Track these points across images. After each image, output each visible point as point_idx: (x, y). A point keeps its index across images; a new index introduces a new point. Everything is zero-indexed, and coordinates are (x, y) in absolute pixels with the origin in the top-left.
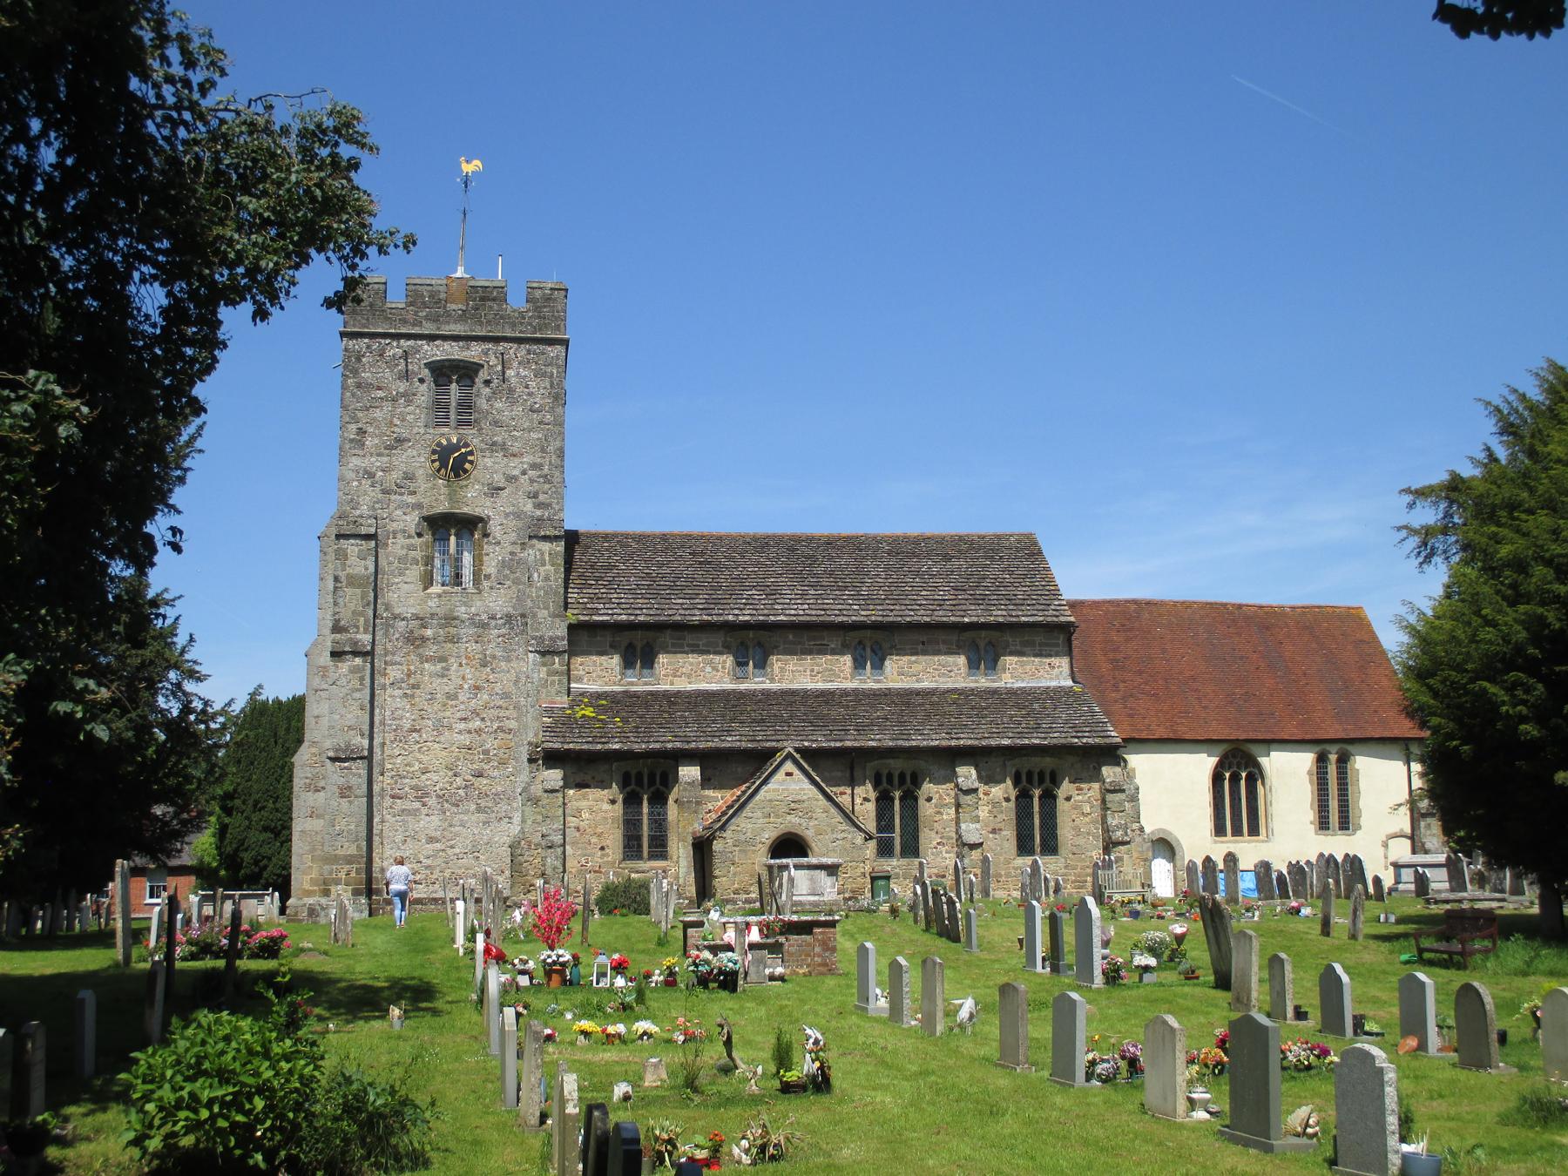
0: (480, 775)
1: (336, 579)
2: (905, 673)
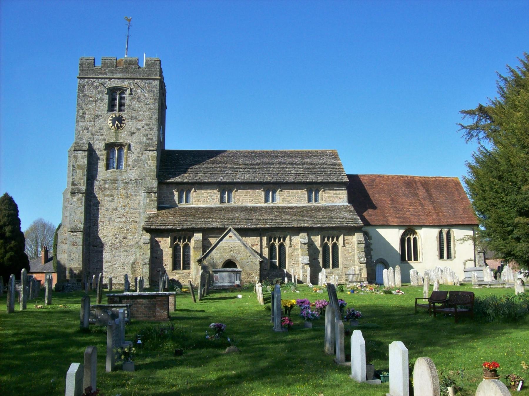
0: (125, 238)
1: (73, 166)
2: (283, 199)
